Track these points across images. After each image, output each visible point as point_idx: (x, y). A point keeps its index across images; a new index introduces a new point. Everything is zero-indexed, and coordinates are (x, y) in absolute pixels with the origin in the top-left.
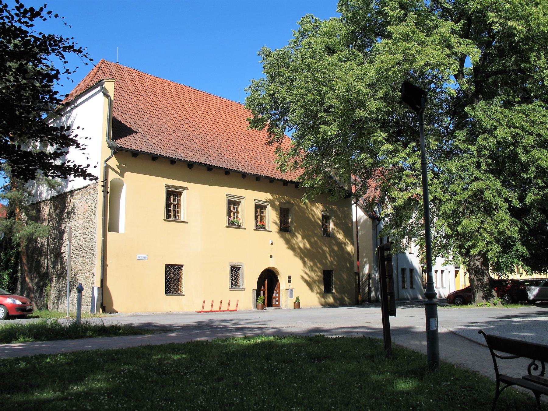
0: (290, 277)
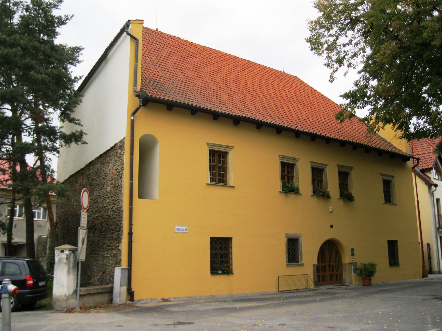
0: (352, 250)
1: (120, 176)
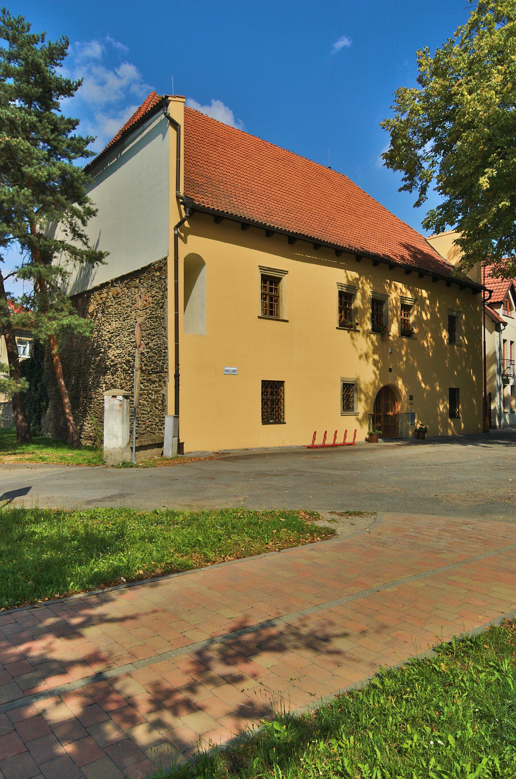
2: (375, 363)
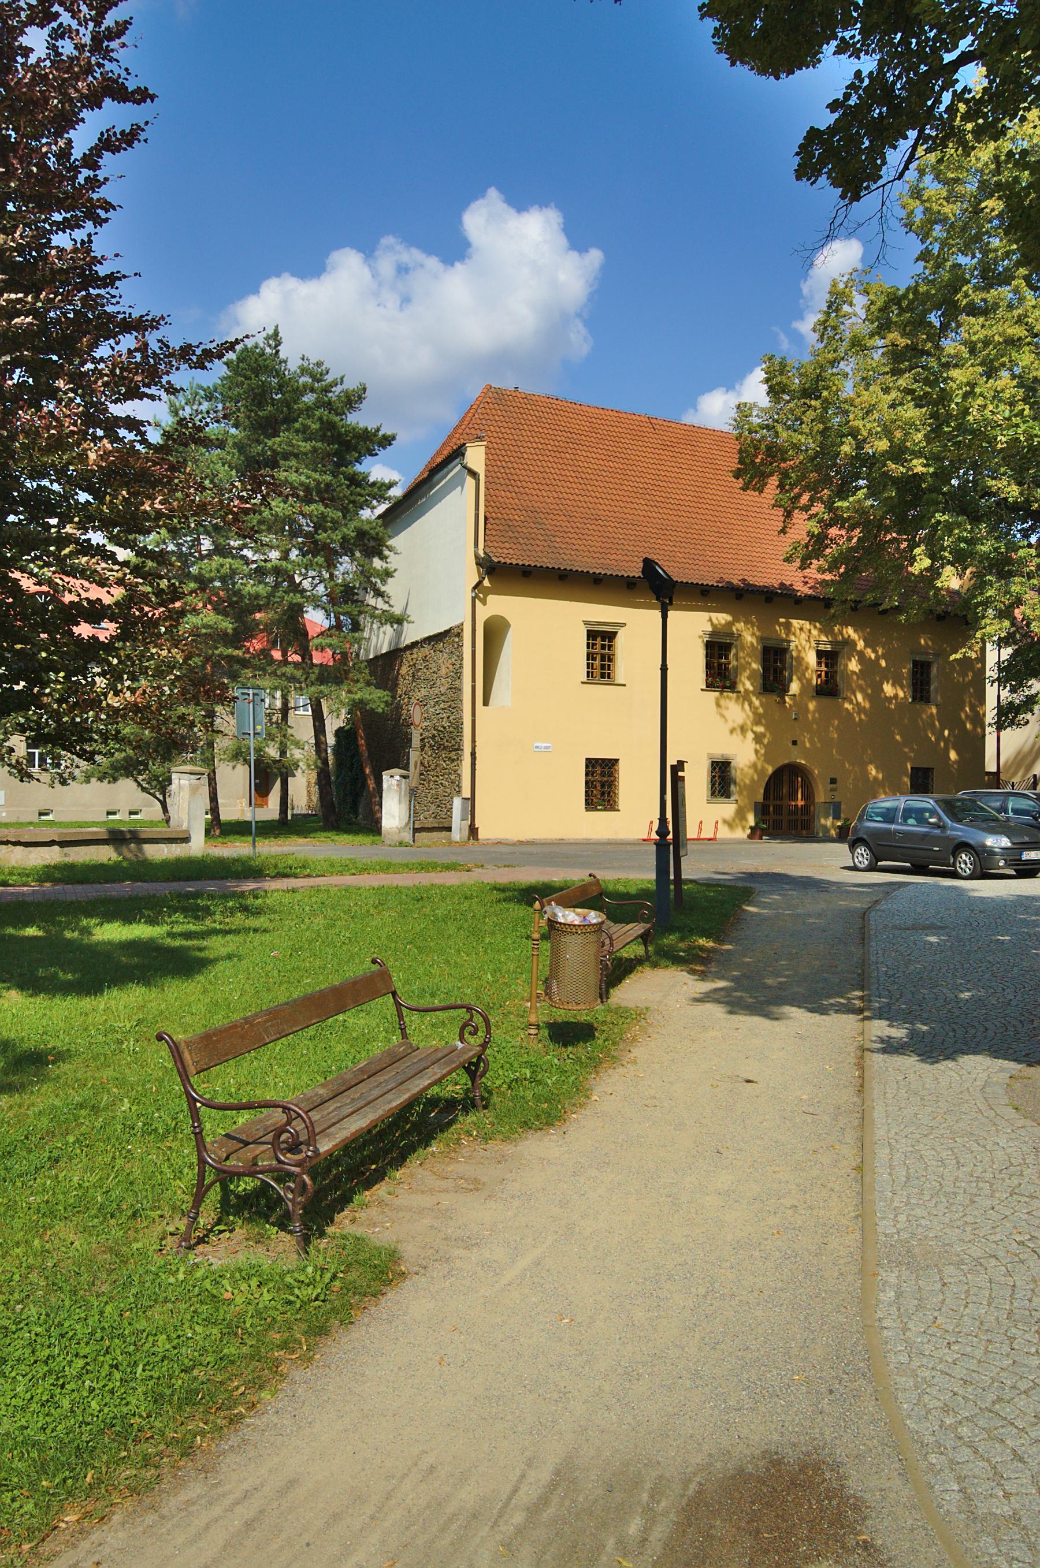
1: (458, 675)
2: (758, 738)
